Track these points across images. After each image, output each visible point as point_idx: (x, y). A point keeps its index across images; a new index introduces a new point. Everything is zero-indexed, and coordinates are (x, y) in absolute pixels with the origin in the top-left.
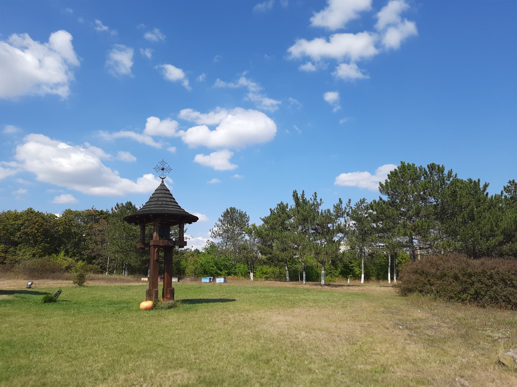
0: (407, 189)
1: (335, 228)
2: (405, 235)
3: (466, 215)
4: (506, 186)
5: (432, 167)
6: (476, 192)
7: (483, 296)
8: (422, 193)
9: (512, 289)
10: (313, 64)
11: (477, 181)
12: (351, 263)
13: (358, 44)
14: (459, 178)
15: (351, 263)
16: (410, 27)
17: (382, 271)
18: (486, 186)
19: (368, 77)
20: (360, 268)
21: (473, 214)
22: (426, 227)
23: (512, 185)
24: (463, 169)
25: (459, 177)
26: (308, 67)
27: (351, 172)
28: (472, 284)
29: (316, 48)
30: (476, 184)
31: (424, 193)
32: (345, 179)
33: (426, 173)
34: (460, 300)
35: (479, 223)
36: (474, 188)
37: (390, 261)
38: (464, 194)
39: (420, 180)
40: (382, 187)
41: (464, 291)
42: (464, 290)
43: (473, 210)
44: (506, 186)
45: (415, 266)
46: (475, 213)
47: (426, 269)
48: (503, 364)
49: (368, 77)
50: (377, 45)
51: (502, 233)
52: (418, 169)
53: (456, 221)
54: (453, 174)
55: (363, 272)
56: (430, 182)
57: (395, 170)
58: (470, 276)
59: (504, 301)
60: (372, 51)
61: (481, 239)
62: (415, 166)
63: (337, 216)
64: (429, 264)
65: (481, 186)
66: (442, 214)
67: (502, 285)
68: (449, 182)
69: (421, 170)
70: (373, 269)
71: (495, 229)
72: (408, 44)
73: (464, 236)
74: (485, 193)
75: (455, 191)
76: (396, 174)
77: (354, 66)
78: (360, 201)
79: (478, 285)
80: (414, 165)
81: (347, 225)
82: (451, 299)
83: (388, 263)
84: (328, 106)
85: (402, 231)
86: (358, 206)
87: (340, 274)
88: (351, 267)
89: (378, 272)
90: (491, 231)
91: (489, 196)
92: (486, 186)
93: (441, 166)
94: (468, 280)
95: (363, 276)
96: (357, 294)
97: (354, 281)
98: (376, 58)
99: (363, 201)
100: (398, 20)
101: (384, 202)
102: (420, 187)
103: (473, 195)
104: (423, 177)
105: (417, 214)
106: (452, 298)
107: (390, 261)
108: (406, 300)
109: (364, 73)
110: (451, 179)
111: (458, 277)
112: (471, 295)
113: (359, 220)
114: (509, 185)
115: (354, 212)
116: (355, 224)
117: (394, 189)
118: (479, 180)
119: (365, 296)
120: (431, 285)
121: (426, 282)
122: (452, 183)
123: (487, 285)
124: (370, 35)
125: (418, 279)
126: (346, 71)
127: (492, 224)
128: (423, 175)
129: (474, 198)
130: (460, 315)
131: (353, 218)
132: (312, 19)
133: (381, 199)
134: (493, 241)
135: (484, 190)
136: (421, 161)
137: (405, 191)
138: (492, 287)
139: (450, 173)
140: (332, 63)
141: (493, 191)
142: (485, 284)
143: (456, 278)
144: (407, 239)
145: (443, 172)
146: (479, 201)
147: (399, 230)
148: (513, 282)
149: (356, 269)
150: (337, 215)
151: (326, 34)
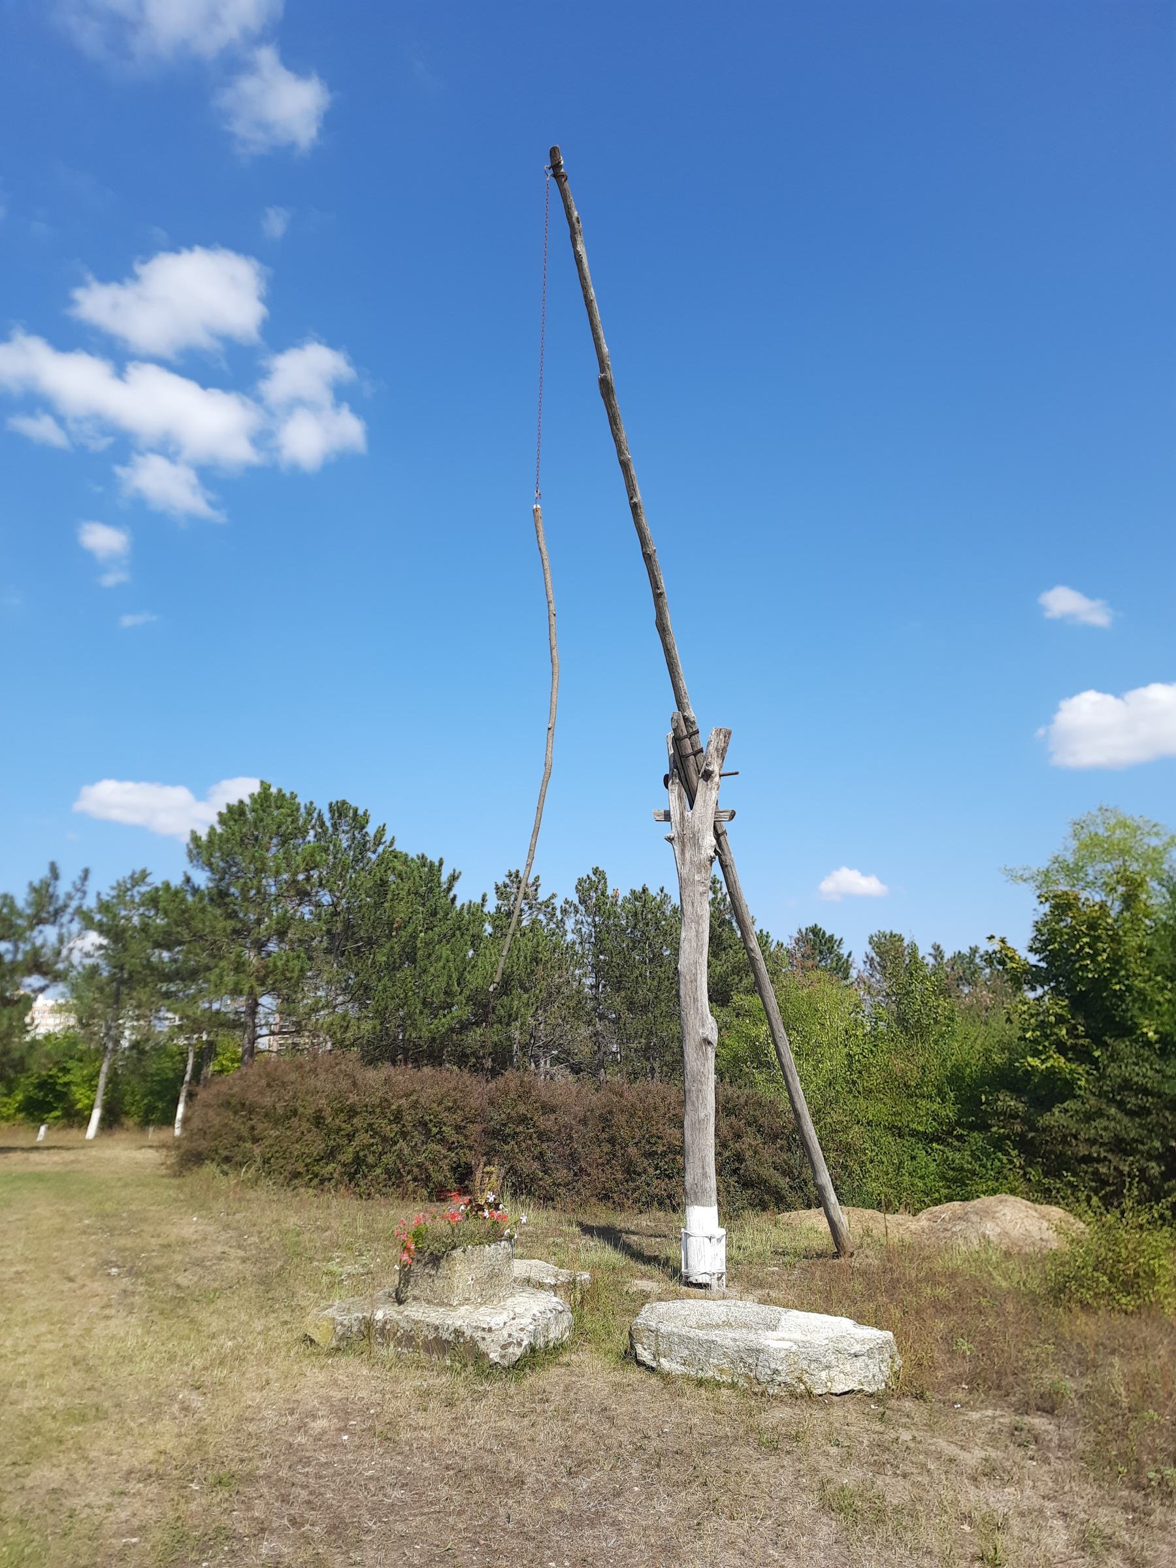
0: (263, 860)
1: (20, 957)
2: (236, 992)
3: (397, 949)
4: (500, 883)
5: (340, 810)
6: (431, 890)
7: (372, 1167)
8: (301, 877)
9: (439, 1147)
10: (60, 421)
11: (437, 864)
12: (66, 1071)
13: (210, 420)
14: (398, 850)
15: (66, 1071)
16: (350, 429)
17: (161, 1099)
18: (454, 878)
19: (219, 517)
20: (94, 1089)
21: (415, 948)
22: (295, 975)
23: (512, 882)
24: (411, 828)
25: (399, 847)
26: (42, 429)
27: (136, 779)
28: (350, 1137)
29: (77, 380)
30: (434, 870)
31: (308, 879)
32: (111, 797)
33: (322, 824)
34: (315, 1182)
35: (425, 971)
36: (428, 881)
37: (189, 1068)
38: (403, 893)
39: (304, 838)
40: (198, 846)
41: (330, 1155)
42: (332, 1152)
43: (416, 938)
44: (500, 883)
45: (224, 1088)
46: (419, 945)
47: (251, 1097)
48: (312, 1341)
49: (219, 517)
50: (262, 438)
51: (469, 999)
52: (302, 810)
53: (374, 963)
54: (387, 838)
55: (98, 1102)
56: (326, 850)
57: (241, 802)
58: (352, 1113)
59: (415, 1179)
60: (241, 452)
61: (421, 1013)
62: (298, 800)
63: (38, 920)
64: (263, 1082)
65: (444, 877)
66: (346, 938)
67: (418, 1137)
68: (373, 857)
69: (309, 814)
70: (135, 1094)
71: (456, 988)
72: (339, 465)
73: (383, 1004)
74: (451, 895)
75: (384, 883)
76: (242, 813)
77: (190, 476)
78: (132, 877)
79: (363, 1138)
80: (294, 796)
81: (64, 952)
82: (296, 1178)
83: (184, 1072)
84: (89, 561)
85: (230, 979)
86: (122, 890)
87: (19, 1110)
88: (67, 1084)
89: (141, 1098)
90: (446, 993)
91: (458, 904)
92: (454, 878)
93: (360, 812)
94: (344, 1126)
95: (96, 1114)
96: (21, 1177)
97: (62, 1133)
98: (251, 471)
99: (140, 878)
100: (326, 398)
101: (196, 891)
102: (299, 858)
103: (423, 897)
104: (312, 833)
105: (281, 934)
106: (296, 1175)
107: (189, 1068)
108: (179, 1187)
109: (211, 504)
110: (380, 849)
111: (323, 1118)
112: (344, 1165)
113: (115, 933)
114: (507, 881)
115: (105, 907)
116: (101, 947)
117: (228, 857)
118: (441, 864)
119: (62, 1184)
120: (256, 1140)
121: (245, 1134)
122: (381, 860)
123: (385, 1139)
124: (244, 405)
125: (226, 1125)
126: (161, 482)
127: (450, 977)
128: (313, 828)
129: (424, 905)
130: (293, 1221)
131: (102, 929)
132: (79, 294)
133: (188, 880)
134: (444, 1022)
135: (449, 889)
136: (315, 793)
137: (258, 865)
138: (396, 1143)
139: (381, 831)
140: (123, 445)
141: (465, 894)
142: (380, 1136)
143: (318, 1120)
144: (241, 1003)
145: (363, 828)
146: (434, 914)
147: (221, 977)
148: (444, 1128)
149: (79, 1094)
150: (36, 916)
151: (118, 355)
